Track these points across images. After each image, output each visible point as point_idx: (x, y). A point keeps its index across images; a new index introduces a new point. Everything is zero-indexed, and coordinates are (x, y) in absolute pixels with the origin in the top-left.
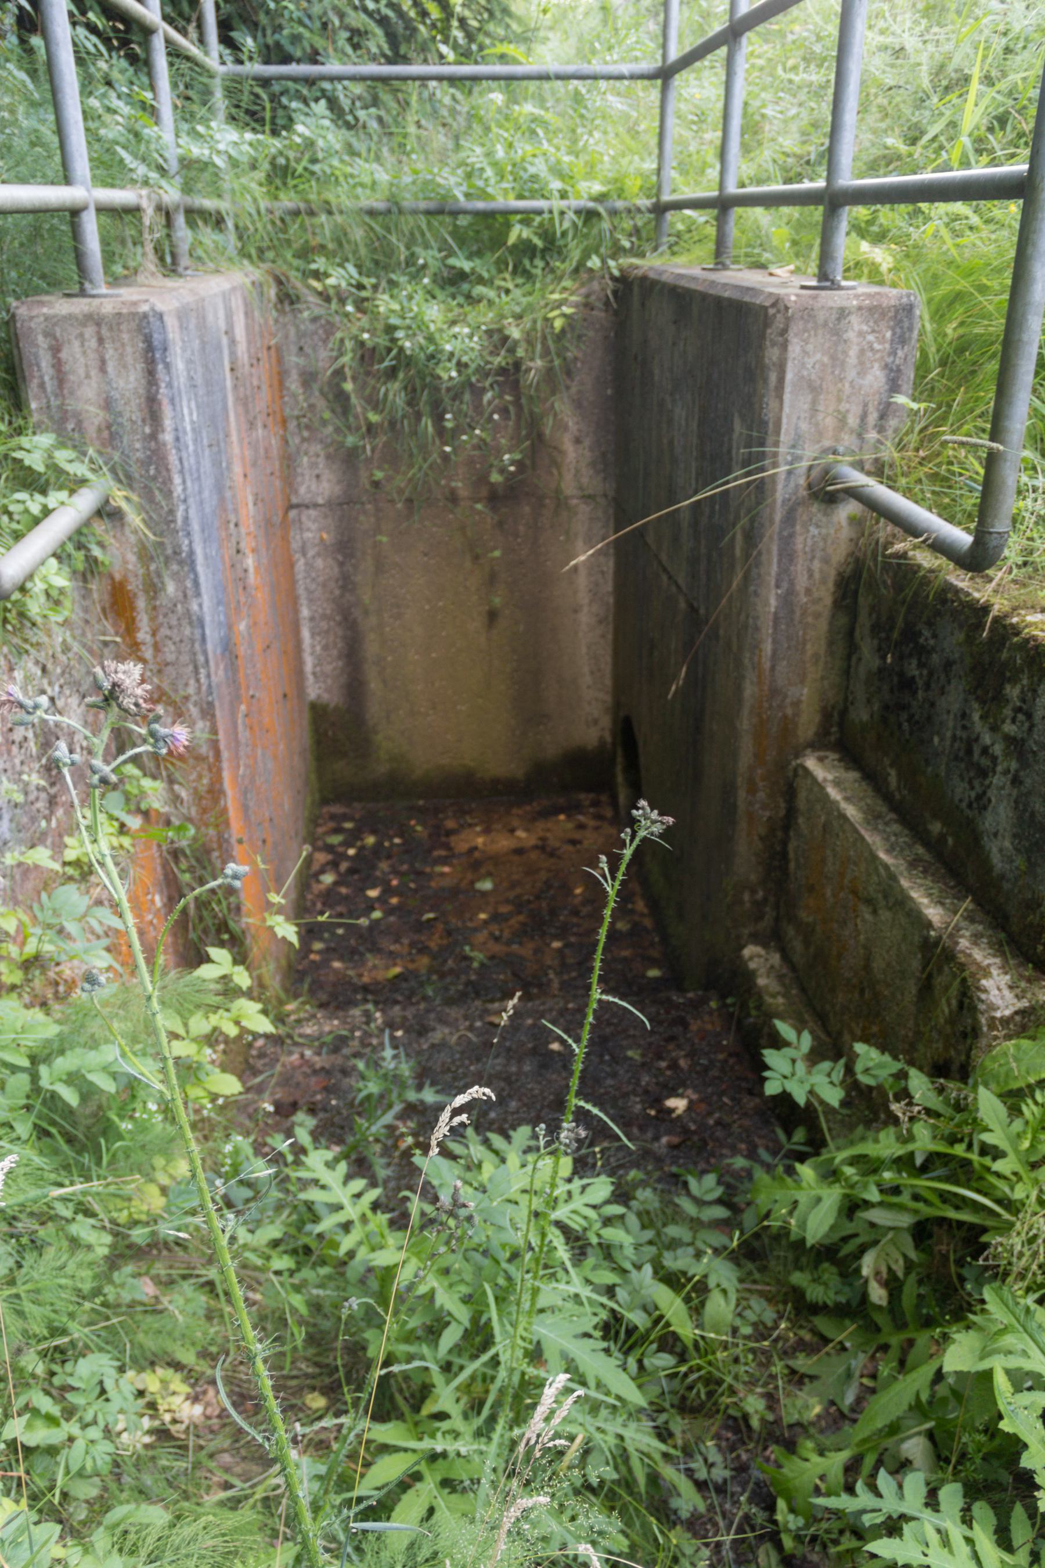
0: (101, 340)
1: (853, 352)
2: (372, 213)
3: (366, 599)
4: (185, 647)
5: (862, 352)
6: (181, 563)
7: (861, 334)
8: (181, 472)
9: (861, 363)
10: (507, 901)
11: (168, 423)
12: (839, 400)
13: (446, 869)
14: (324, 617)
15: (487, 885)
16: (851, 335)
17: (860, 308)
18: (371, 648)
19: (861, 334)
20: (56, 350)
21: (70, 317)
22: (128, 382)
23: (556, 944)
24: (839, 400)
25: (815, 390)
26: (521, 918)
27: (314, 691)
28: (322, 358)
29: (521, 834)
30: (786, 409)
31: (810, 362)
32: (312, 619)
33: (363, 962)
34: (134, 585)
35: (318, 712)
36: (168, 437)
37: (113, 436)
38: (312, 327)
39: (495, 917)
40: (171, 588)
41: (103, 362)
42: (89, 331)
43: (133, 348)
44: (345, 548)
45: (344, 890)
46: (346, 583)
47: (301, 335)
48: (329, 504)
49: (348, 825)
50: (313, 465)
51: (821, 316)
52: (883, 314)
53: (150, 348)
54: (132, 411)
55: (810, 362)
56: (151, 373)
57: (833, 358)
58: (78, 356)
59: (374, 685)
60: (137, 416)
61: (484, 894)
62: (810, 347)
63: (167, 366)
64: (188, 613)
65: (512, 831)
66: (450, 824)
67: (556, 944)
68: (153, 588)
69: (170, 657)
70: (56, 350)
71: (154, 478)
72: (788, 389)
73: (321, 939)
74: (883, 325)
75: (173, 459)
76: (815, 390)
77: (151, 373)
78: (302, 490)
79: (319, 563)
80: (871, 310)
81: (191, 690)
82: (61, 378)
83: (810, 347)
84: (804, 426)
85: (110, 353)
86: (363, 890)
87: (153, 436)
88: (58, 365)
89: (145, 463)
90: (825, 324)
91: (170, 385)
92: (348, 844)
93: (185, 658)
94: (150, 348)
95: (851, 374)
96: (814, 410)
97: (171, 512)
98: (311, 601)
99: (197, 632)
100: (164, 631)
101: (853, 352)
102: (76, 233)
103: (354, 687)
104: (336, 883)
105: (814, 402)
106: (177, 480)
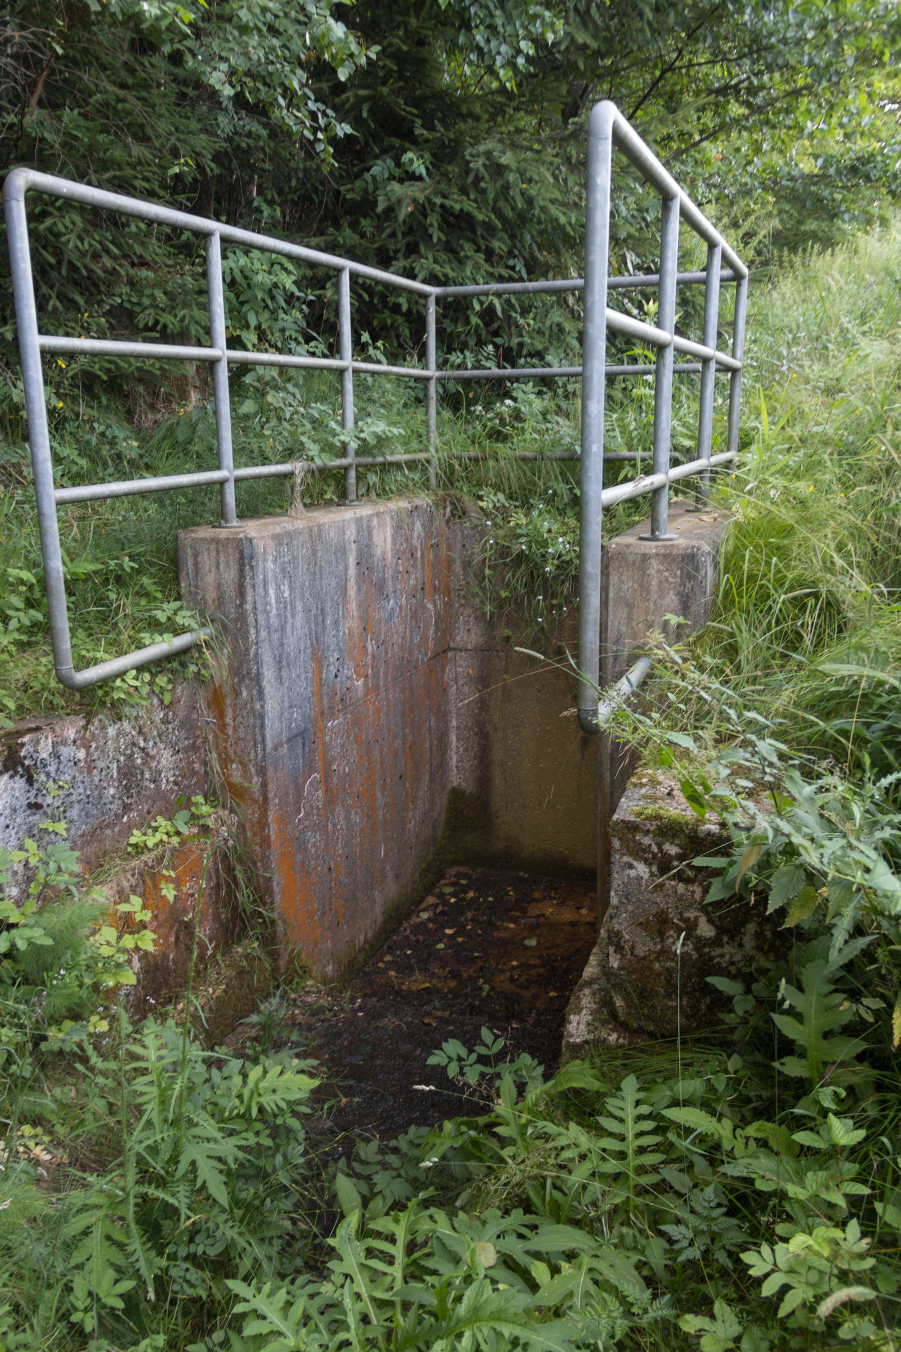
0: (218, 552)
1: (654, 583)
2: (524, 459)
3: (496, 718)
4: (250, 731)
5: (660, 583)
6: (251, 679)
7: (658, 571)
8: (256, 627)
9: (661, 590)
10: (540, 957)
11: (249, 599)
12: (647, 613)
13: (512, 926)
14: (467, 727)
15: (532, 942)
16: (652, 571)
17: (657, 555)
18: (498, 754)
19: (658, 571)
20: (196, 556)
21: (204, 539)
22: (230, 575)
23: (553, 994)
24: (647, 613)
25: (630, 606)
26: (541, 970)
27: (455, 779)
28: (477, 554)
29: (584, 911)
30: (611, 617)
31: (625, 587)
32: (458, 728)
33: (410, 974)
34: (226, 689)
35: (456, 794)
36: (248, 607)
37: (220, 604)
38: (471, 532)
39: (525, 967)
40: (244, 694)
41: (218, 564)
42: (213, 547)
43: (234, 557)
44: (483, 680)
45: (431, 925)
46: (483, 704)
47: (464, 537)
48: (475, 650)
49: (463, 882)
50: (467, 622)
51: (631, 559)
52: (674, 560)
53: (242, 557)
54: (230, 591)
55: (625, 587)
56: (242, 571)
57: (641, 585)
58: (206, 560)
59: (497, 781)
60: (233, 594)
61: (527, 948)
62: (624, 578)
63: (252, 567)
64: (253, 710)
65: (579, 908)
66: (537, 895)
67: (553, 994)
68: (237, 694)
69: (242, 735)
70: (196, 556)
71: (239, 630)
72: (611, 604)
73: (393, 954)
74: (674, 566)
75: (251, 619)
76: (630, 606)
77: (242, 571)
78: (458, 639)
79: (466, 689)
80: (665, 556)
81: (252, 756)
82: (197, 572)
83: (624, 578)
84: (623, 629)
85: (222, 559)
86: (444, 928)
87: (241, 606)
88: (196, 564)
89: (236, 620)
90: (634, 564)
91: (252, 578)
92: (453, 895)
93: (249, 737)
94: (242, 557)
95: (655, 596)
96: (630, 619)
97: (247, 649)
98: (458, 715)
99: (258, 722)
100: (239, 719)
101: (654, 583)
102: (222, 492)
103: (484, 781)
104: (429, 920)
105: (630, 614)
106: (252, 631)
